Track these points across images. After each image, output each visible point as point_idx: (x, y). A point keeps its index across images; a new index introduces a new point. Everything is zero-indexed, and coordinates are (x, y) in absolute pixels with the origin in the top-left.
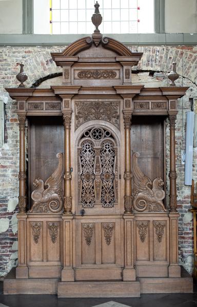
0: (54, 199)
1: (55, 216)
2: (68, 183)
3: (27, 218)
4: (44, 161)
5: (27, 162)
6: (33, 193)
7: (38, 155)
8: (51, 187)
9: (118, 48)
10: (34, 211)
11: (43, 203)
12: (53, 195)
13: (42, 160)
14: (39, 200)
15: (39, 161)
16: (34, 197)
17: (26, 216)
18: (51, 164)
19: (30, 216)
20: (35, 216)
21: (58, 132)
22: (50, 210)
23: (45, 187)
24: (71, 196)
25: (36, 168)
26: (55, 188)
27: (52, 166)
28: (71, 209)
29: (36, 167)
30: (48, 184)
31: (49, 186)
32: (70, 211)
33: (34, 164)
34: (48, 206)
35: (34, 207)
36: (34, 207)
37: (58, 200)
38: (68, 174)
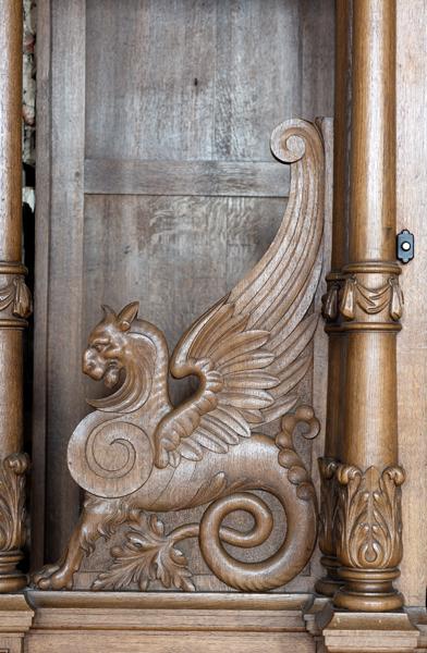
0: (246, 487)
1: (251, 618)
2: (372, 351)
3: (35, 627)
4: (141, 216)
5: (31, 181)
6: (79, 433)
7: (104, 169)
8: (227, 390)
9: (312, 250)
10: (84, 580)
11: (155, 510)
12: (236, 451)
13: (129, 209)
14: (132, 486)
15: (110, 215)
16: (86, 465)
17: (24, 619)
18: (193, 236)
19: (53, 617)
20: (93, 617)
21: (87, 191)
22: (213, 570)
23: (184, 389)
24: (395, 464)
25: (87, 267)
26: (257, 399)
27: (199, 249)
28: (394, 568)
29: (86, 258)
30: (202, 366)
31: (209, 385)
32: (388, 590)
33: (76, 236)
34: (200, 537)
35: (89, 548)
36: (89, 548)
37: (273, 491)
38: (374, 280)
